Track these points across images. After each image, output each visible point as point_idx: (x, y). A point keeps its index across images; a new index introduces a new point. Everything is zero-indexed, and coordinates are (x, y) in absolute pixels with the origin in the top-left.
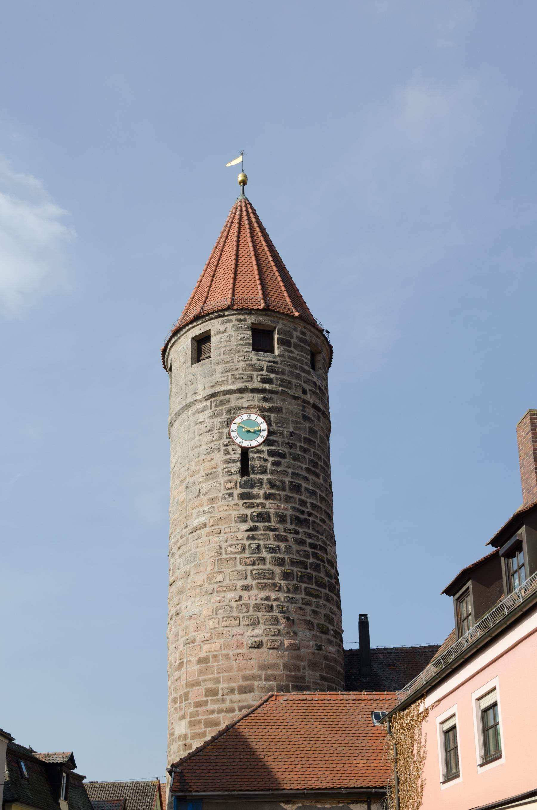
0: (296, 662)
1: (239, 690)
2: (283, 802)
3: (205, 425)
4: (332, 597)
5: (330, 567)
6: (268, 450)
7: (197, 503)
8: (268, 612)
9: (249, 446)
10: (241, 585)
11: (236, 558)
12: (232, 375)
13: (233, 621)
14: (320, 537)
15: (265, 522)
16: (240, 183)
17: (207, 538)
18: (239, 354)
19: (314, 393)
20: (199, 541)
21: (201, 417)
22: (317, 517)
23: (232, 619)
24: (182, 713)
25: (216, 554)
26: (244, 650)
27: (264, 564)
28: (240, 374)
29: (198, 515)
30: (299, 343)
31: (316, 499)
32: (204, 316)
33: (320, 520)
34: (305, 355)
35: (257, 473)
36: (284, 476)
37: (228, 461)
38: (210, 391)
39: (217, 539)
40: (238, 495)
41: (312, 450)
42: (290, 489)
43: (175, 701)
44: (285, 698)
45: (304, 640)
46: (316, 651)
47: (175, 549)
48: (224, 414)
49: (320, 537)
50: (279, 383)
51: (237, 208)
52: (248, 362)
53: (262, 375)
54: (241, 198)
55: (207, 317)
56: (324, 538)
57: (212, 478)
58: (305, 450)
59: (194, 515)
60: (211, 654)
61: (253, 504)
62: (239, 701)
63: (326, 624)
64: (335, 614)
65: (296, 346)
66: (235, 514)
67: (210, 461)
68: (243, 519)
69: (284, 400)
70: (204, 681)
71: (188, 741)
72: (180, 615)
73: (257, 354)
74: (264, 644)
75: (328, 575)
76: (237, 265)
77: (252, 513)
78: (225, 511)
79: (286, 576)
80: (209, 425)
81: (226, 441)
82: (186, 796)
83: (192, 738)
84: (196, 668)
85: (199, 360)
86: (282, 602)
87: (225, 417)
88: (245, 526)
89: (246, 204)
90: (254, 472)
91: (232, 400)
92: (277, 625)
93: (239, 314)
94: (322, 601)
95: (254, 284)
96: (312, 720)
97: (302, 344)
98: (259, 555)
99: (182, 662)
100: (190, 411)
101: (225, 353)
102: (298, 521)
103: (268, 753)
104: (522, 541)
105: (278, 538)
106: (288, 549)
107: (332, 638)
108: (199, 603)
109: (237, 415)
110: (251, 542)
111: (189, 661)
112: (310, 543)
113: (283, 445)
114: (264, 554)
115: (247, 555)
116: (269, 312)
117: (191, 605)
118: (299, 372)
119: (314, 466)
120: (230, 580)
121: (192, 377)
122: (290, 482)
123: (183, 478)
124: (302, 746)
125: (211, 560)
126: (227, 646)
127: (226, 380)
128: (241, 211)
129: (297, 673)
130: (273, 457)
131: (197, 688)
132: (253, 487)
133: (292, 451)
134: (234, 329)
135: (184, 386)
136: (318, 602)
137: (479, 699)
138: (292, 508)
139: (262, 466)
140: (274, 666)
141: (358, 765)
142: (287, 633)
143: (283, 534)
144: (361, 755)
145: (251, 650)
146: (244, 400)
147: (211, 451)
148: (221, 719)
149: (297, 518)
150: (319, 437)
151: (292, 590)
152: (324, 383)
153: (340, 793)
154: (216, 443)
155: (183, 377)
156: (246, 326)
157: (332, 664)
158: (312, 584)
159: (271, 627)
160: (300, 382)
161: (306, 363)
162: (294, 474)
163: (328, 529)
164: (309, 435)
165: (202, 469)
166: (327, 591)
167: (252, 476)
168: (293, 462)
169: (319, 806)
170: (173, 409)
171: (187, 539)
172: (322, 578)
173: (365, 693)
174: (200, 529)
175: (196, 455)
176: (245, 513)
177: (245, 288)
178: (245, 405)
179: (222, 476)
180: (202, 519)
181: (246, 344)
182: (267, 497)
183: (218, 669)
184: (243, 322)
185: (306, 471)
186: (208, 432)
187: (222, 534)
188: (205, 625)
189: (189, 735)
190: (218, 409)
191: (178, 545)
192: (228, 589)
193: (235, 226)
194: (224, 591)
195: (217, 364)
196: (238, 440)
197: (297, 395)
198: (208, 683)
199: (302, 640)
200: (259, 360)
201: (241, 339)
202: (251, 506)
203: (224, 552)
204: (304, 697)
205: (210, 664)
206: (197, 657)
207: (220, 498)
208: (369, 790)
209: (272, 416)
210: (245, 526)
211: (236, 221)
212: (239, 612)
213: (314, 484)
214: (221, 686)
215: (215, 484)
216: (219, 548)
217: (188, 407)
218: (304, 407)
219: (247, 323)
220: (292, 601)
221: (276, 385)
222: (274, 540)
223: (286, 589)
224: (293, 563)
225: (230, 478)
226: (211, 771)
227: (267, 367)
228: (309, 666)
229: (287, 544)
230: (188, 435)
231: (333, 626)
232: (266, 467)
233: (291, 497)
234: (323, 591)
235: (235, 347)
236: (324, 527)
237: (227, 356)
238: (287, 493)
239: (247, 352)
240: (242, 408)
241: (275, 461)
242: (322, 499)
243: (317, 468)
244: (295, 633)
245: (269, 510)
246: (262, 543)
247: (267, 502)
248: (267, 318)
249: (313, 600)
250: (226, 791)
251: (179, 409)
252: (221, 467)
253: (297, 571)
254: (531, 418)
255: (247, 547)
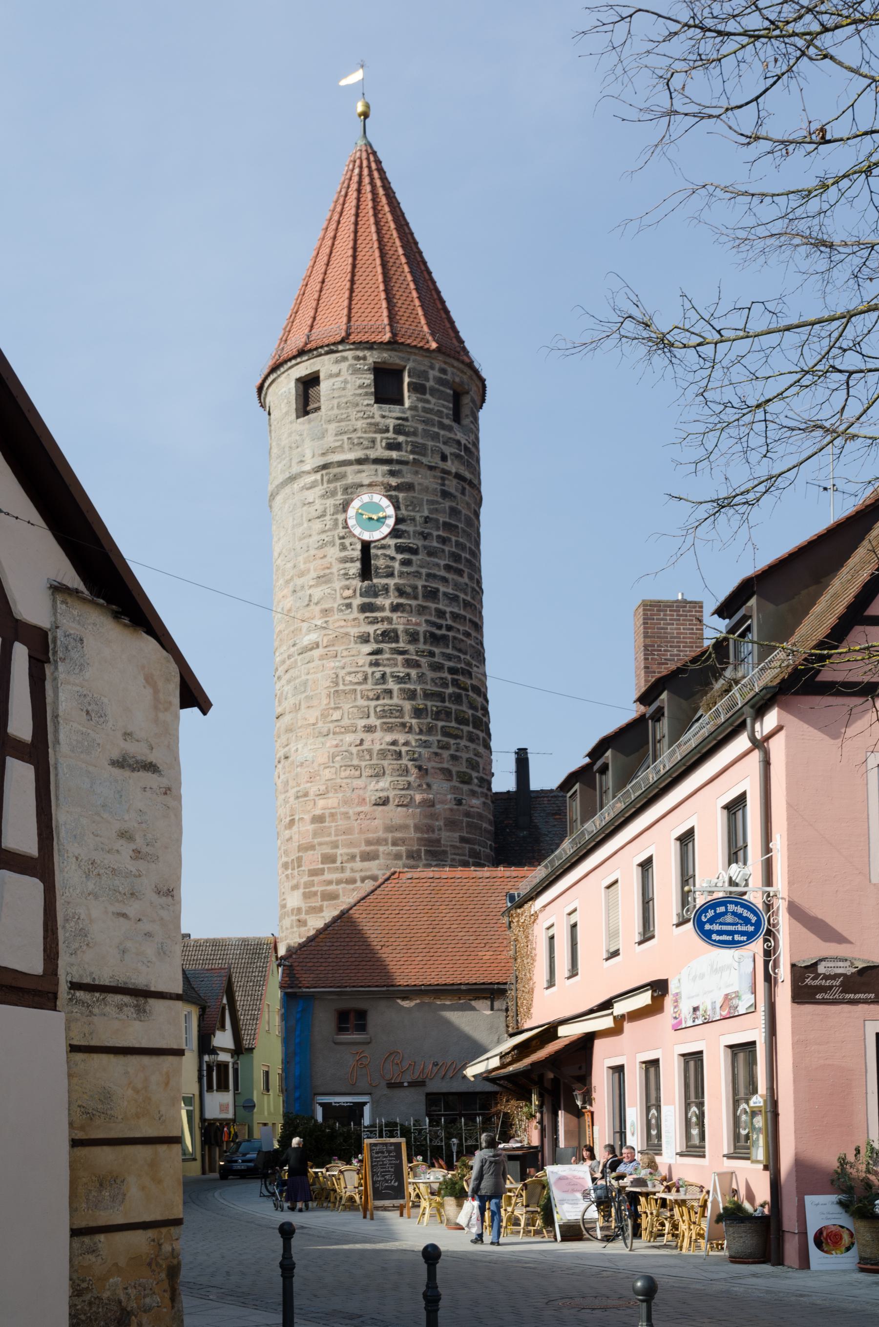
0: (429, 822)
1: (361, 857)
2: (399, 998)
3: (316, 507)
4: (477, 735)
5: (475, 696)
6: (396, 544)
7: (307, 615)
8: (396, 759)
9: (372, 539)
10: (363, 725)
11: (355, 690)
12: (349, 439)
13: (353, 771)
14: (462, 657)
15: (392, 642)
16: (360, 115)
17: (320, 662)
18: (357, 409)
19: (457, 456)
20: (311, 665)
21: (312, 495)
22: (458, 630)
23: (352, 768)
24: (295, 882)
25: (332, 685)
26: (367, 808)
27: (391, 698)
28: (359, 438)
29: (309, 631)
30: (437, 386)
31: (459, 606)
32: (310, 351)
33: (464, 634)
34: (446, 403)
35: (381, 577)
36: (416, 579)
37: (345, 560)
38: (321, 461)
39: (332, 664)
40: (358, 606)
41: (454, 539)
42: (424, 596)
43: (285, 866)
44: (409, 875)
45: (440, 794)
46: (455, 807)
47: (281, 670)
48: (340, 493)
49: (462, 657)
50: (409, 448)
51: (355, 162)
52: (369, 421)
53: (387, 438)
54: (361, 142)
55: (315, 352)
56: (468, 657)
57: (326, 582)
58: (444, 540)
59: (304, 630)
60: (327, 812)
61: (376, 618)
62: (361, 870)
63: (469, 771)
64: (481, 757)
65: (433, 392)
66: (355, 631)
67: (322, 558)
68: (365, 639)
69: (416, 473)
70: (320, 844)
71: (303, 916)
72: (290, 759)
73: (381, 408)
74: (391, 799)
75: (473, 706)
76: (354, 266)
77: (376, 630)
78: (342, 627)
79: (418, 713)
80: (320, 508)
81: (341, 532)
82: (295, 993)
83: (307, 913)
84: (311, 827)
85: (306, 413)
86: (412, 747)
87: (340, 498)
88: (367, 648)
89: (368, 154)
90: (378, 576)
91: (349, 474)
92: (406, 776)
93: (356, 349)
94: (463, 743)
95: (377, 298)
96: (438, 903)
97: (441, 388)
98: (384, 687)
99: (294, 819)
100: (295, 485)
101: (338, 407)
102: (434, 639)
103: (387, 944)
104: (663, 708)
105: (409, 663)
106: (421, 677)
107: (476, 789)
108: (312, 747)
109: (355, 496)
110: (374, 669)
111: (302, 818)
112: (449, 668)
113: (414, 536)
114: (391, 685)
115: (369, 686)
116: (396, 346)
117: (303, 748)
118: (436, 430)
119: (455, 561)
120: (349, 719)
121: (298, 438)
122: (424, 587)
123: (289, 577)
124: (425, 935)
125: (326, 691)
126: (346, 802)
127: (341, 446)
128: (361, 167)
129: (431, 835)
130: (401, 553)
131: (312, 852)
132: (376, 595)
133: (427, 543)
134: (350, 372)
135: (287, 449)
136: (458, 744)
137: (570, 914)
138: (427, 621)
139: (388, 567)
140: (404, 827)
141: (484, 958)
142: (419, 786)
143: (414, 657)
144: (488, 945)
145: (375, 807)
146: (364, 474)
147: (323, 545)
148: (341, 892)
149: (433, 635)
150: (463, 518)
151: (425, 730)
152: (472, 437)
153: (460, 989)
154: (329, 533)
155: (286, 435)
156: (366, 367)
157: (475, 821)
158: (451, 722)
159: (399, 778)
160: (438, 444)
161: (447, 415)
162: (429, 576)
163: (474, 644)
164: (450, 519)
165: (312, 568)
166: (470, 729)
167: (375, 581)
168: (428, 559)
169: (439, 1003)
170: (275, 477)
171: (296, 661)
172: (464, 712)
173: (502, 869)
174: (312, 649)
175: (305, 548)
176: (367, 631)
177: (365, 306)
178: (366, 482)
179: (338, 579)
180: (313, 637)
181: (366, 394)
182: (395, 608)
183: (336, 830)
184: (362, 361)
185: (445, 569)
186: (318, 518)
187: (339, 658)
188: (320, 775)
189: (304, 909)
190: (332, 486)
191: (285, 667)
192: (347, 730)
193: (353, 195)
194: (342, 733)
195: (329, 421)
196: (357, 531)
197: (433, 464)
198: (324, 846)
199: (437, 793)
200: (383, 417)
201: (360, 387)
202: (375, 621)
203: (341, 682)
204: (431, 875)
205: (326, 824)
206: (311, 815)
207: (335, 610)
208: (491, 986)
209: (401, 495)
210: (367, 648)
211: (354, 186)
212: (361, 760)
213: (456, 586)
214: (340, 851)
215: (329, 591)
216: (334, 676)
217: (292, 479)
218: (443, 479)
219: (367, 362)
220: (425, 744)
221: (406, 451)
222: (403, 666)
223: (417, 730)
224: (427, 695)
225: (347, 583)
226: (324, 964)
227: (394, 427)
228: (445, 825)
229: (419, 670)
230: (294, 519)
231: (478, 772)
232: (393, 567)
233: (424, 608)
234: (465, 728)
235: (352, 398)
236: (469, 642)
237: (342, 411)
238: (420, 602)
239: (368, 405)
240: (362, 486)
241: (405, 559)
242: (467, 604)
243: (461, 563)
244: (429, 785)
245: (397, 626)
246: (388, 670)
247: (395, 616)
248: (393, 354)
249: (452, 741)
250: (339, 987)
251: (281, 480)
252: (336, 567)
253: (432, 706)
254: (644, 610)
255: (370, 676)
